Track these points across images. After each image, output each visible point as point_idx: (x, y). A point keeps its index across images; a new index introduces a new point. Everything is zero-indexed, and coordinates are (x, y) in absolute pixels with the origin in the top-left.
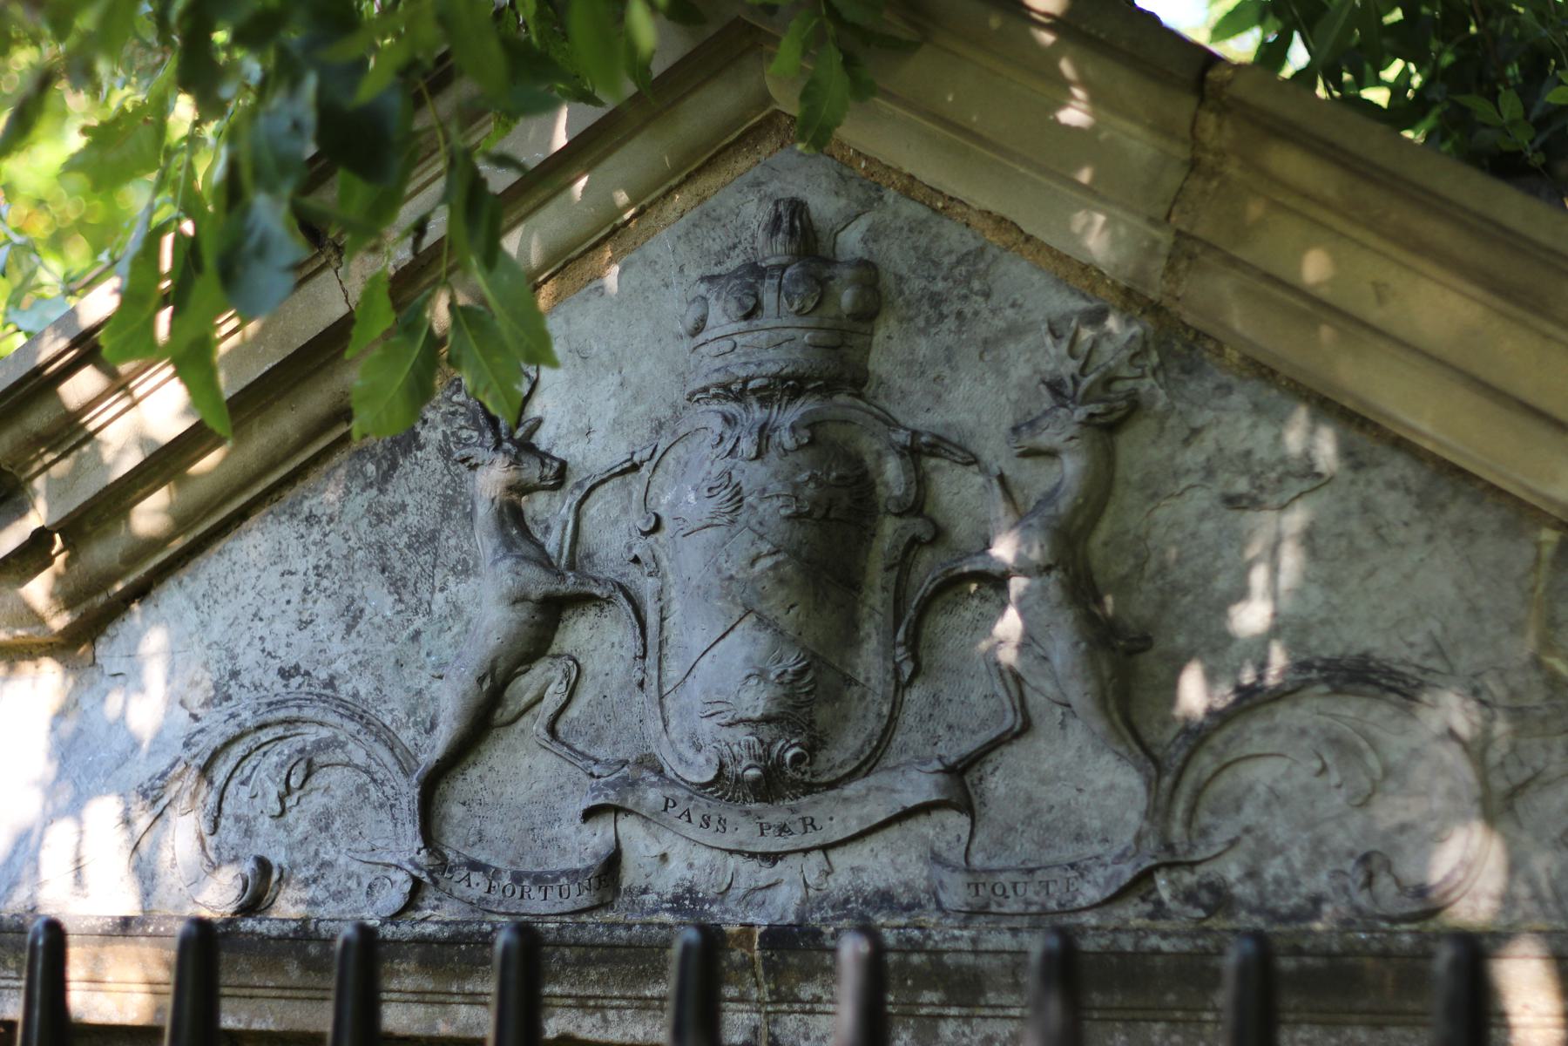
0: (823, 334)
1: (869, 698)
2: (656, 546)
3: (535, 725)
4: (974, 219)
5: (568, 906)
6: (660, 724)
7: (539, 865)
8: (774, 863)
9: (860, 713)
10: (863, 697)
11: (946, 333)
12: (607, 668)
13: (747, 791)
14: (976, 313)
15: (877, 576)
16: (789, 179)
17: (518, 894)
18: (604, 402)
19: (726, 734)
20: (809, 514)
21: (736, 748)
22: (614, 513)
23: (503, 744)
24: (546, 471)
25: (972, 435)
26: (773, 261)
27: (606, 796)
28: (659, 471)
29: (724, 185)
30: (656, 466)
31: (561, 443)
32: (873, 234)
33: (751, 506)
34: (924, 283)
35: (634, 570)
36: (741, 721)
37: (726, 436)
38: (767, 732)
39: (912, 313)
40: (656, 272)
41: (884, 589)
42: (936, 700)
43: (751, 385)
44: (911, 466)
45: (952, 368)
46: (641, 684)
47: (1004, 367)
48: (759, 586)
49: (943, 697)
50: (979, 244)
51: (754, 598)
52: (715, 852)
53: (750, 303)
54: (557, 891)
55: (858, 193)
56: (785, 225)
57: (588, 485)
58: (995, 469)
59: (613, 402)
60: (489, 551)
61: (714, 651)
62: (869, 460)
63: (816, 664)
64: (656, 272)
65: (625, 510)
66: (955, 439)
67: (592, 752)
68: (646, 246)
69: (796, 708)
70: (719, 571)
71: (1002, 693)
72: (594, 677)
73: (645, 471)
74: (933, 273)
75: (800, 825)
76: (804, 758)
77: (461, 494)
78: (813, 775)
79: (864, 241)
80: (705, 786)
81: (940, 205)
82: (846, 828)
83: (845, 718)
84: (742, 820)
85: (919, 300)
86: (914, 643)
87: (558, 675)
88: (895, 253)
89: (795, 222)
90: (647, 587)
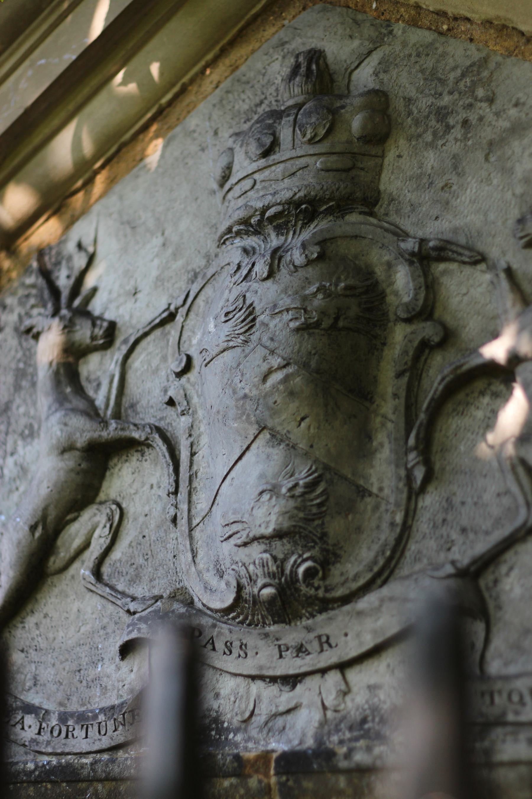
0: (334, 158)
1: (383, 507)
2: (188, 386)
3: (83, 570)
4: (477, 33)
5: (105, 742)
6: (189, 555)
7: (83, 705)
8: (294, 687)
9: (373, 524)
10: (376, 507)
11: (452, 145)
12: (147, 509)
13: (265, 613)
14: (481, 119)
15: (389, 382)
16: (309, 34)
17: (63, 734)
18: (148, 262)
19: (242, 554)
20: (317, 324)
21: (251, 568)
22: (155, 362)
23: (56, 591)
24: (97, 330)
25: (479, 233)
26: (291, 103)
27: (139, 630)
28: (192, 315)
29: (253, 52)
30: (189, 310)
31: (112, 306)
32: (385, 66)
33: (265, 325)
34: (431, 100)
35: (170, 411)
36: (255, 539)
37: (243, 265)
38: (280, 548)
39: (420, 130)
40: (194, 139)
41: (395, 396)
42: (449, 504)
43: (267, 214)
44: (419, 272)
45: (458, 174)
46: (174, 520)
47: (509, 165)
48: (271, 401)
49: (457, 500)
50: (483, 55)
51: (267, 413)
52: (239, 680)
53: (268, 140)
54: (96, 728)
55: (368, 31)
56: (303, 69)
57: (132, 340)
58: (503, 264)
59: (156, 262)
60: (46, 408)
61: (233, 474)
62: (380, 272)
63: (328, 476)
64: (194, 139)
65: (164, 359)
66: (462, 240)
67: (131, 591)
68: (188, 119)
69: (308, 520)
70: (234, 392)
71: (515, 489)
72: (135, 519)
73: (179, 318)
74: (440, 89)
75: (316, 645)
76: (317, 572)
77: (30, 365)
78: (327, 590)
79: (376, 74)
80: (227, 611)
81: (445, 27)
82: (361, 644)
83: (359, 530)
84: (261, 643)
85: (428, 116)
86: (426, 448)
87: (102, 519)
88: (404, 80)
89: (318, 75)
90: (178, 425)
